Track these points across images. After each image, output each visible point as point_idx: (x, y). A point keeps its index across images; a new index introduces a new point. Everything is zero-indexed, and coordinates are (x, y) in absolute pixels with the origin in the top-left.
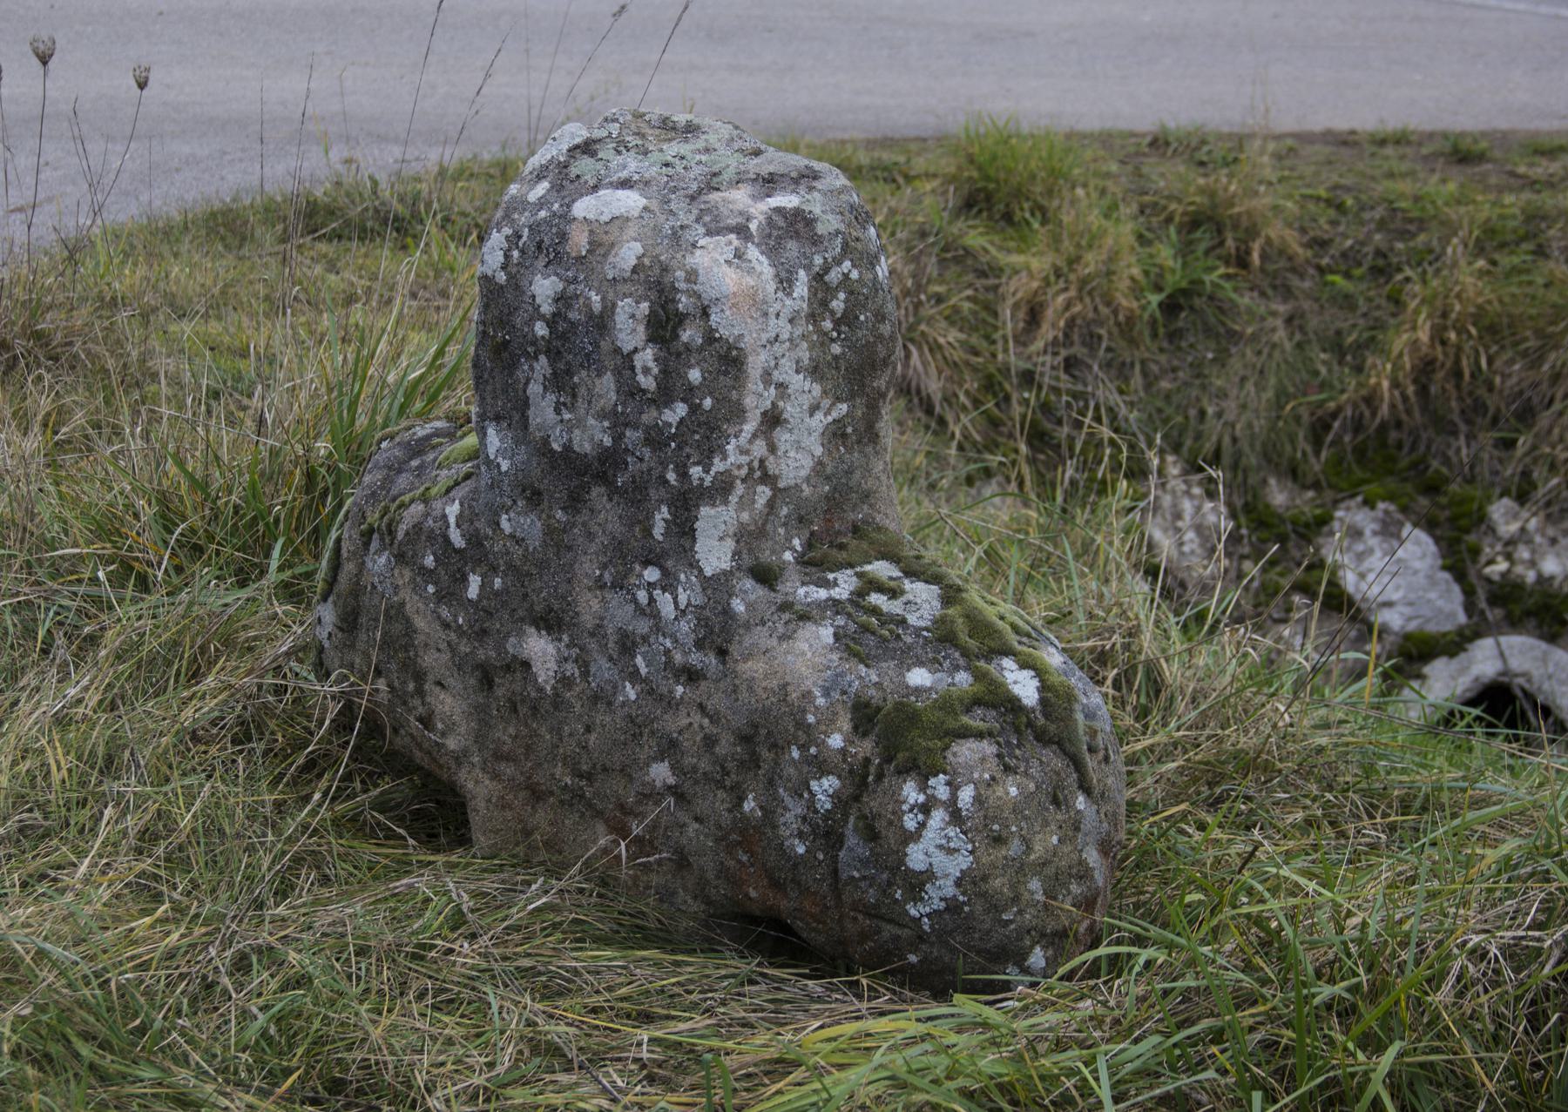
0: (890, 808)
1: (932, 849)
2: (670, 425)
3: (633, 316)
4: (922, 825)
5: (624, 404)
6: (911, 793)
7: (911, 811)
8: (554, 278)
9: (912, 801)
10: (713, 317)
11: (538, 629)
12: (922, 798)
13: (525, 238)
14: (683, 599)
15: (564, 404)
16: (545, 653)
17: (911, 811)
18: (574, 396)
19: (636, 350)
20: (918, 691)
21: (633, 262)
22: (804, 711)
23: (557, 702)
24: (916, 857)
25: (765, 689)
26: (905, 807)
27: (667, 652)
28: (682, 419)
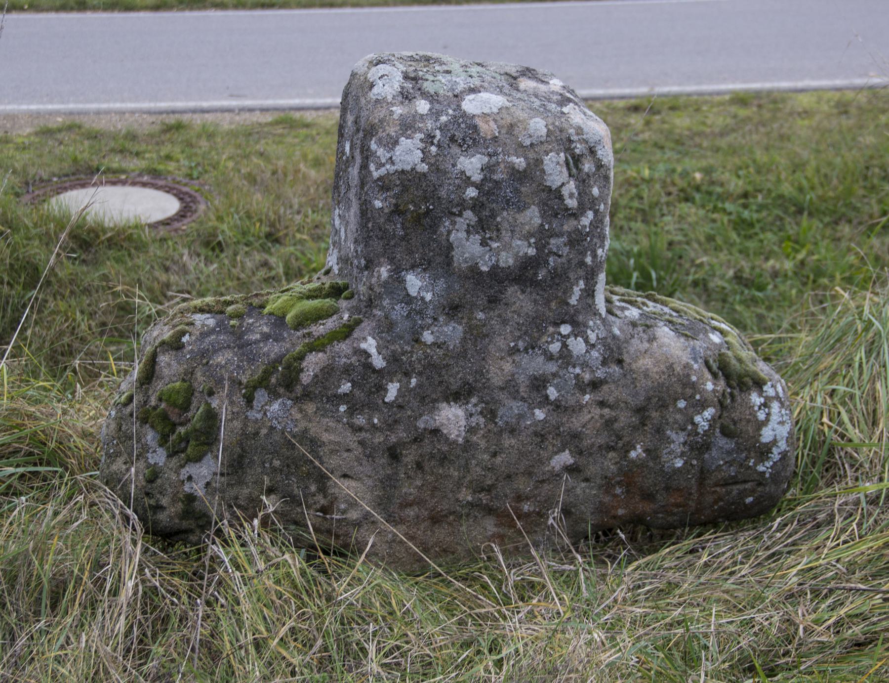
0: (748, 412)
1: (776, 426)
2: (585, 226)
3: (558, 163)
4: (768, 414)
5: (550, 223)
6: (756, 399)
7: (760, 408)
8: (478, 156)
9: (759, 404)
10: (599, 152)
11: (448, 403)
12: (762, 400)
13: (438, 137)
14: (592, 337)
15: (490, 238)
16: (457, 416)
17: (760, 408)
18: (498, 230)
19: (563, 184)
20: (379, 420)
21: (546, 130)
22: (688, 376)
23: (468, 445)
24: (767, 435)
25: (657, 372)
26: (756, 408)
27: (577, 376)
28: (591, 222)
